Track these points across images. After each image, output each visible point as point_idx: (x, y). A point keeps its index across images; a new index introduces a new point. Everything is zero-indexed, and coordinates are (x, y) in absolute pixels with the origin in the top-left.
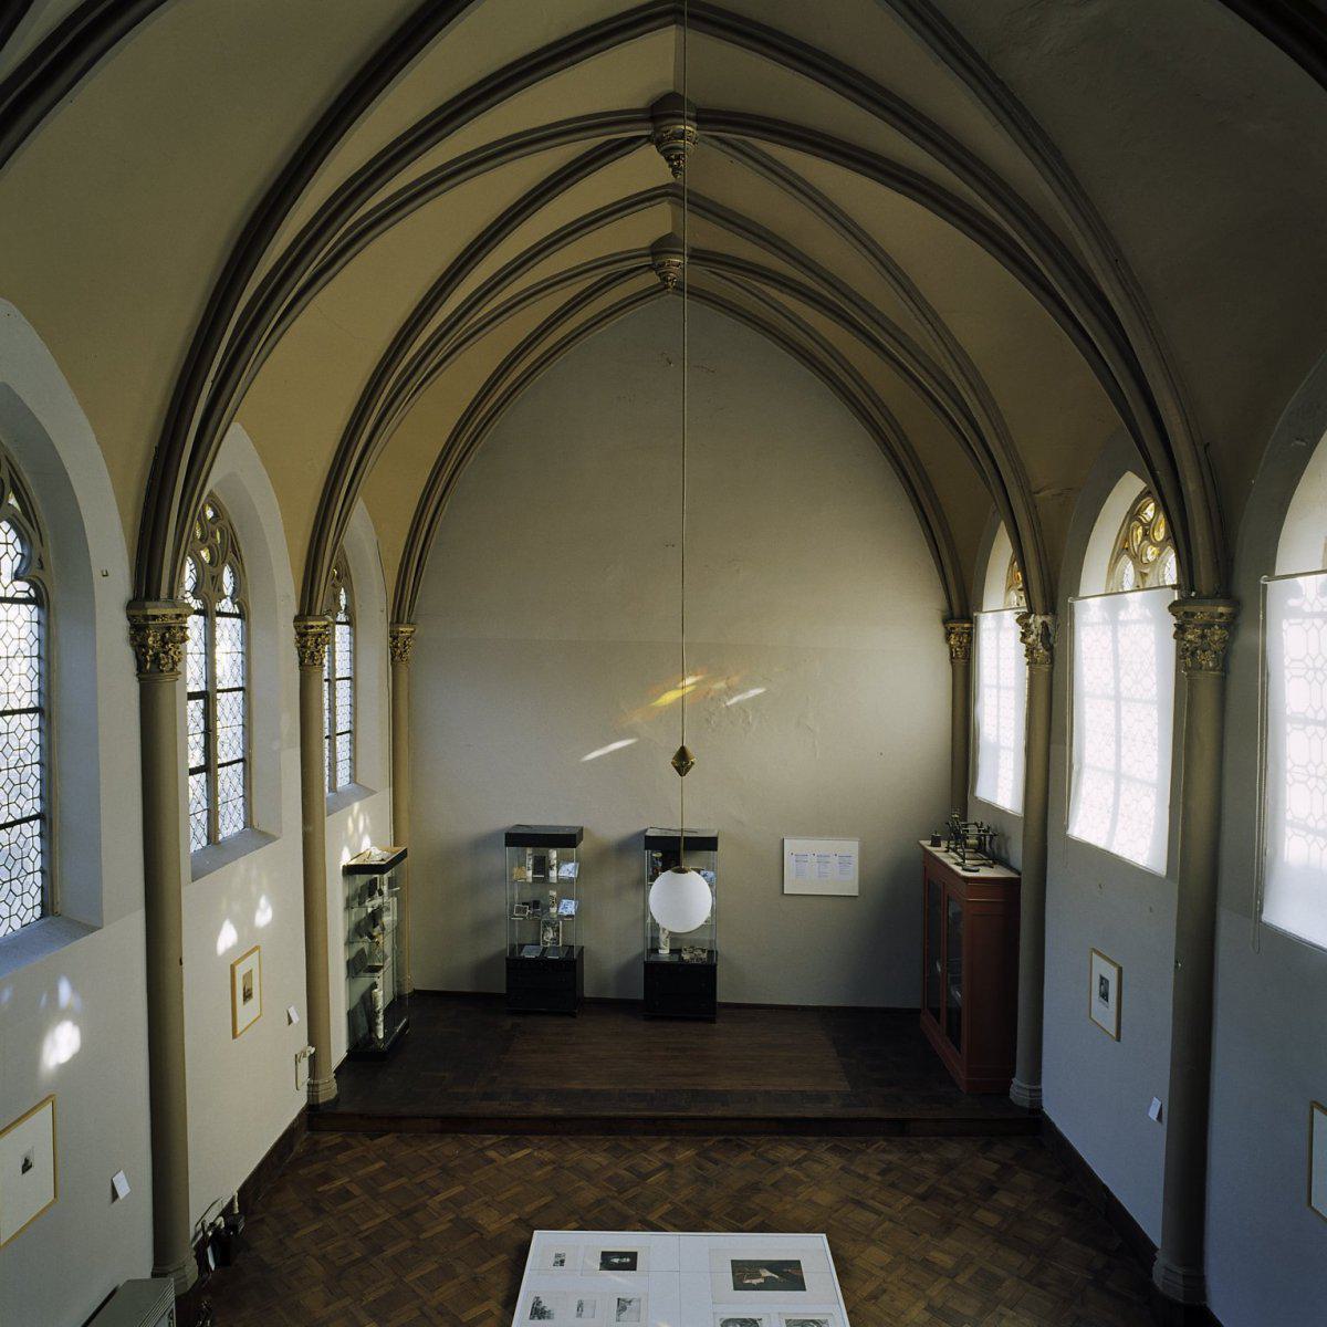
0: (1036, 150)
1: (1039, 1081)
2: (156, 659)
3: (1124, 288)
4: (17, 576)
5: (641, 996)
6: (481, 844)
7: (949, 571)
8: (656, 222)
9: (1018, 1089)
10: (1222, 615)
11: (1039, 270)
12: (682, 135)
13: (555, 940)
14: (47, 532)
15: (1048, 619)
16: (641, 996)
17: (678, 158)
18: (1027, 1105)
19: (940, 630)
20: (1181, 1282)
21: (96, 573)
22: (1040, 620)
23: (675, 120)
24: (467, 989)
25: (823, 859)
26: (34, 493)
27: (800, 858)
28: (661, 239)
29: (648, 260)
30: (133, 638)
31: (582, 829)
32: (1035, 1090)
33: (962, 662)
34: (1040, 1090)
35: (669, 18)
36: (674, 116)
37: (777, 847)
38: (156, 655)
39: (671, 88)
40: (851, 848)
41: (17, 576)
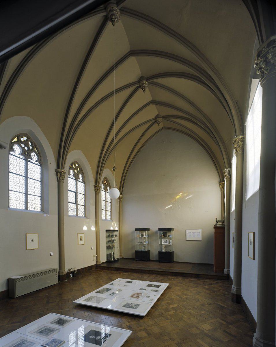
0: (179, 39)
1: (229, 269)
2: (59, 178)
3: (213, 72)
4: (37, 161)
5: (158, 260)
6: (132, 232)
7: (220, 172)
8: (152, 112)
9: (225, 271)
10: (241, 138)
11: (203, 81)
12: (144, 83)
13: (145, 249)
14: (42, 156)
15: (229, 169)
16: (158, 260)
17: (144, 88)
18: (226, 273)
19: (218, 185)
20: (235, 289)
21: (49, 163)
22: (227, 170)
23: (143, 81)
24: (131, 258)
25: (194, 233)
26: (39, 150)
27: (190, 233)
28: (156, 116)
29: (155, 121)
30: (56, 175)
31: (173, 252)
32: (228, 270)
33: (222, 191)
34: (229, 270)
35: (130, 55)
36: (142, 80)
37: (185, 231)
38: (59, 177)
39: (141, 75)
40: (200, 231)
41: (37, 161)
